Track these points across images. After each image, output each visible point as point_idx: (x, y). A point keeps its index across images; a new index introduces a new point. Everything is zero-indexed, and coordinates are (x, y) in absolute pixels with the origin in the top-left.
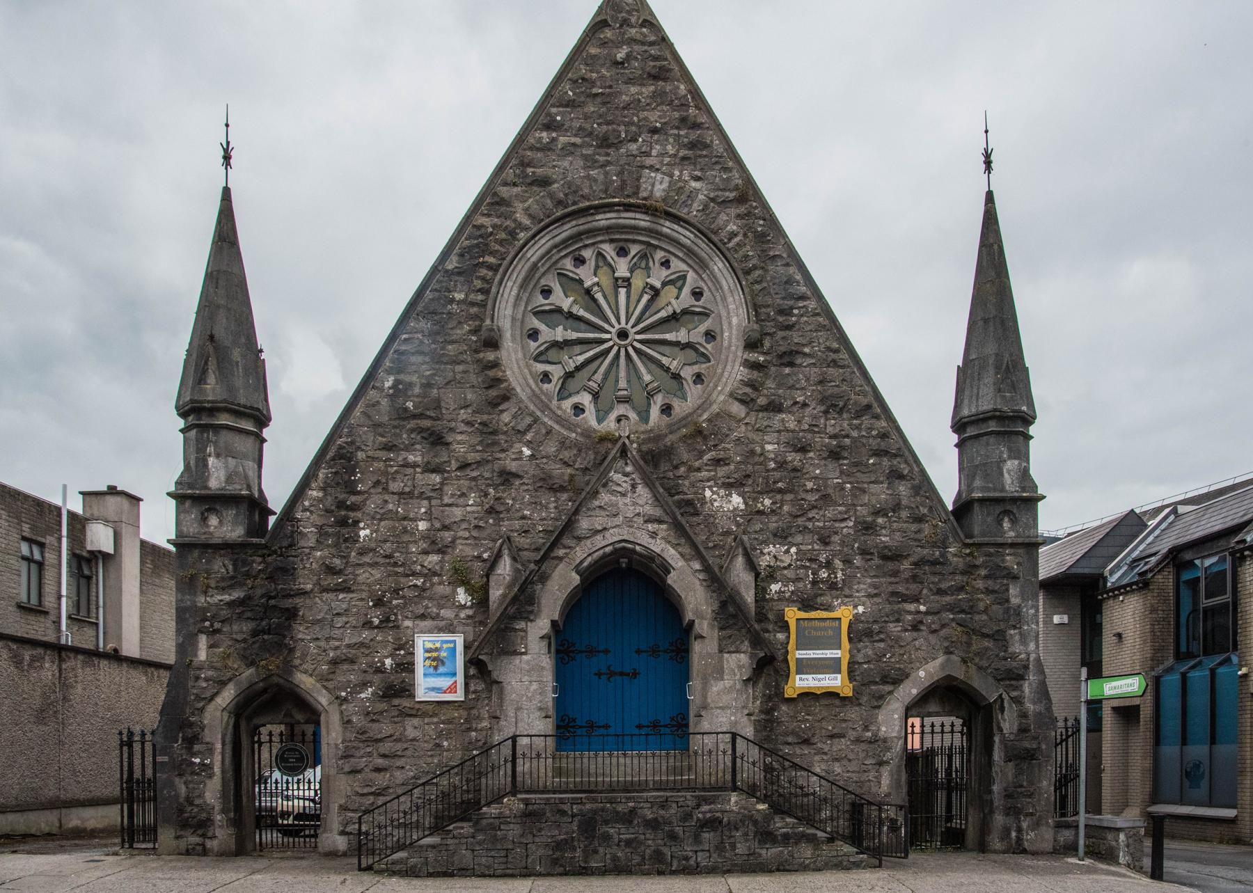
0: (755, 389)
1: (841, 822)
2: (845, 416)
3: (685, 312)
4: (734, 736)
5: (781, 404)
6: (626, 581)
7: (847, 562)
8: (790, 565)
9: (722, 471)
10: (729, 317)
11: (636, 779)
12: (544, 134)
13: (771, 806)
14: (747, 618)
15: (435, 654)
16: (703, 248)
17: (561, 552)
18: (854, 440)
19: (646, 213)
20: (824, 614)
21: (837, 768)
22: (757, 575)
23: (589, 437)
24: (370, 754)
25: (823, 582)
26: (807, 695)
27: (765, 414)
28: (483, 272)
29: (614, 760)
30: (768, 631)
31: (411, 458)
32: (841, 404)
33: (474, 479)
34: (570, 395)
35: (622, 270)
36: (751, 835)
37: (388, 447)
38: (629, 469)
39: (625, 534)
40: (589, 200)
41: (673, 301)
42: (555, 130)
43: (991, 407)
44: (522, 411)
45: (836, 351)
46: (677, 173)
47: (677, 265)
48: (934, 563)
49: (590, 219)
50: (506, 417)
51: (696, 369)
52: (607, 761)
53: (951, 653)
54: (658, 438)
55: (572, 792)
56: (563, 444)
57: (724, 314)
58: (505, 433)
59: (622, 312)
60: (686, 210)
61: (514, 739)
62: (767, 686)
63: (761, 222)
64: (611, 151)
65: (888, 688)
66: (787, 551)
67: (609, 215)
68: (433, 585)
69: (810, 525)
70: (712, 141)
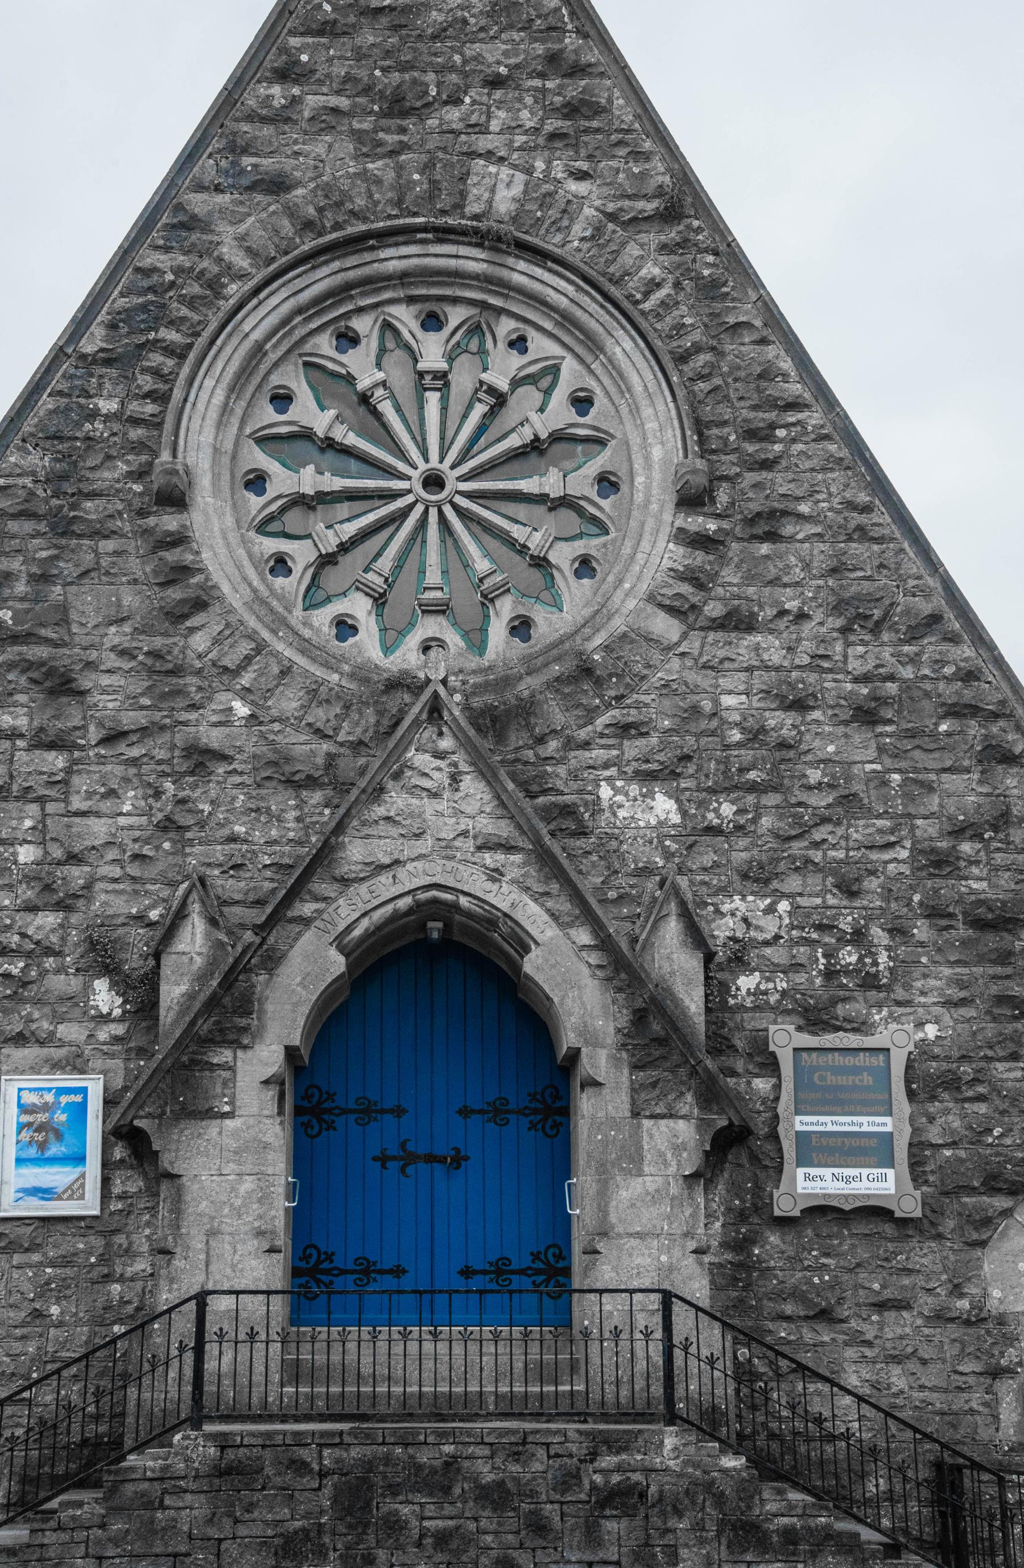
0: (699, 585)
1: (913, 1507)
2: (886, 637)
3: (558, 437)
4: (668, 1298)
5: (753, 615)
6: (440, 968)
7: (898, 931)
8: (777, 937)
9: (633, 748)
10: (645, 446)
11: (458, 1390)
12: (276, 90)
14: (687, 1044)
15: (41, 1118)
16: (592, 312)
17: (307, 909)
18: (907, 686)
19: (479, 245)
20: (852, 1040)
21: (897, 1378)
22: (709, 958)
23: (365, 681)
25: (847, 973)
26: (822, 1212)
27: (720, 635)
28: (156, 359)
29: (413, 1347)
30: (733, 1073)
32: (877, 613)
33: (134, 762)
34: (328, 600)
35: (432, 352)
36: (712, 1528)
38: (446, 743)
39: (437, 871)
40: (365, 220)
41: (534, 417)
42: (296, 82)
44: (232, 630)
45: (866, 509)
46: (540, 165)
47: (541, 346)
49: (367, 257)
50: (200, 642)
51: (580, 547)
52: (398, 1349)
54: (506, 682)
55: (322, 1418)
56: (314, 694)
57: (635, 440)
58: (199, 672)
59: (432, 438)
60: (558, 238)
61: (201, 1299)
62: (735, 1189)
63: (710, 259)
64: (409, 123)
65: (1001, 1202)
66: (770, 910)
67: (405, 250)
68: (43, 973)
69: (817, 856)
70: (610, 101)
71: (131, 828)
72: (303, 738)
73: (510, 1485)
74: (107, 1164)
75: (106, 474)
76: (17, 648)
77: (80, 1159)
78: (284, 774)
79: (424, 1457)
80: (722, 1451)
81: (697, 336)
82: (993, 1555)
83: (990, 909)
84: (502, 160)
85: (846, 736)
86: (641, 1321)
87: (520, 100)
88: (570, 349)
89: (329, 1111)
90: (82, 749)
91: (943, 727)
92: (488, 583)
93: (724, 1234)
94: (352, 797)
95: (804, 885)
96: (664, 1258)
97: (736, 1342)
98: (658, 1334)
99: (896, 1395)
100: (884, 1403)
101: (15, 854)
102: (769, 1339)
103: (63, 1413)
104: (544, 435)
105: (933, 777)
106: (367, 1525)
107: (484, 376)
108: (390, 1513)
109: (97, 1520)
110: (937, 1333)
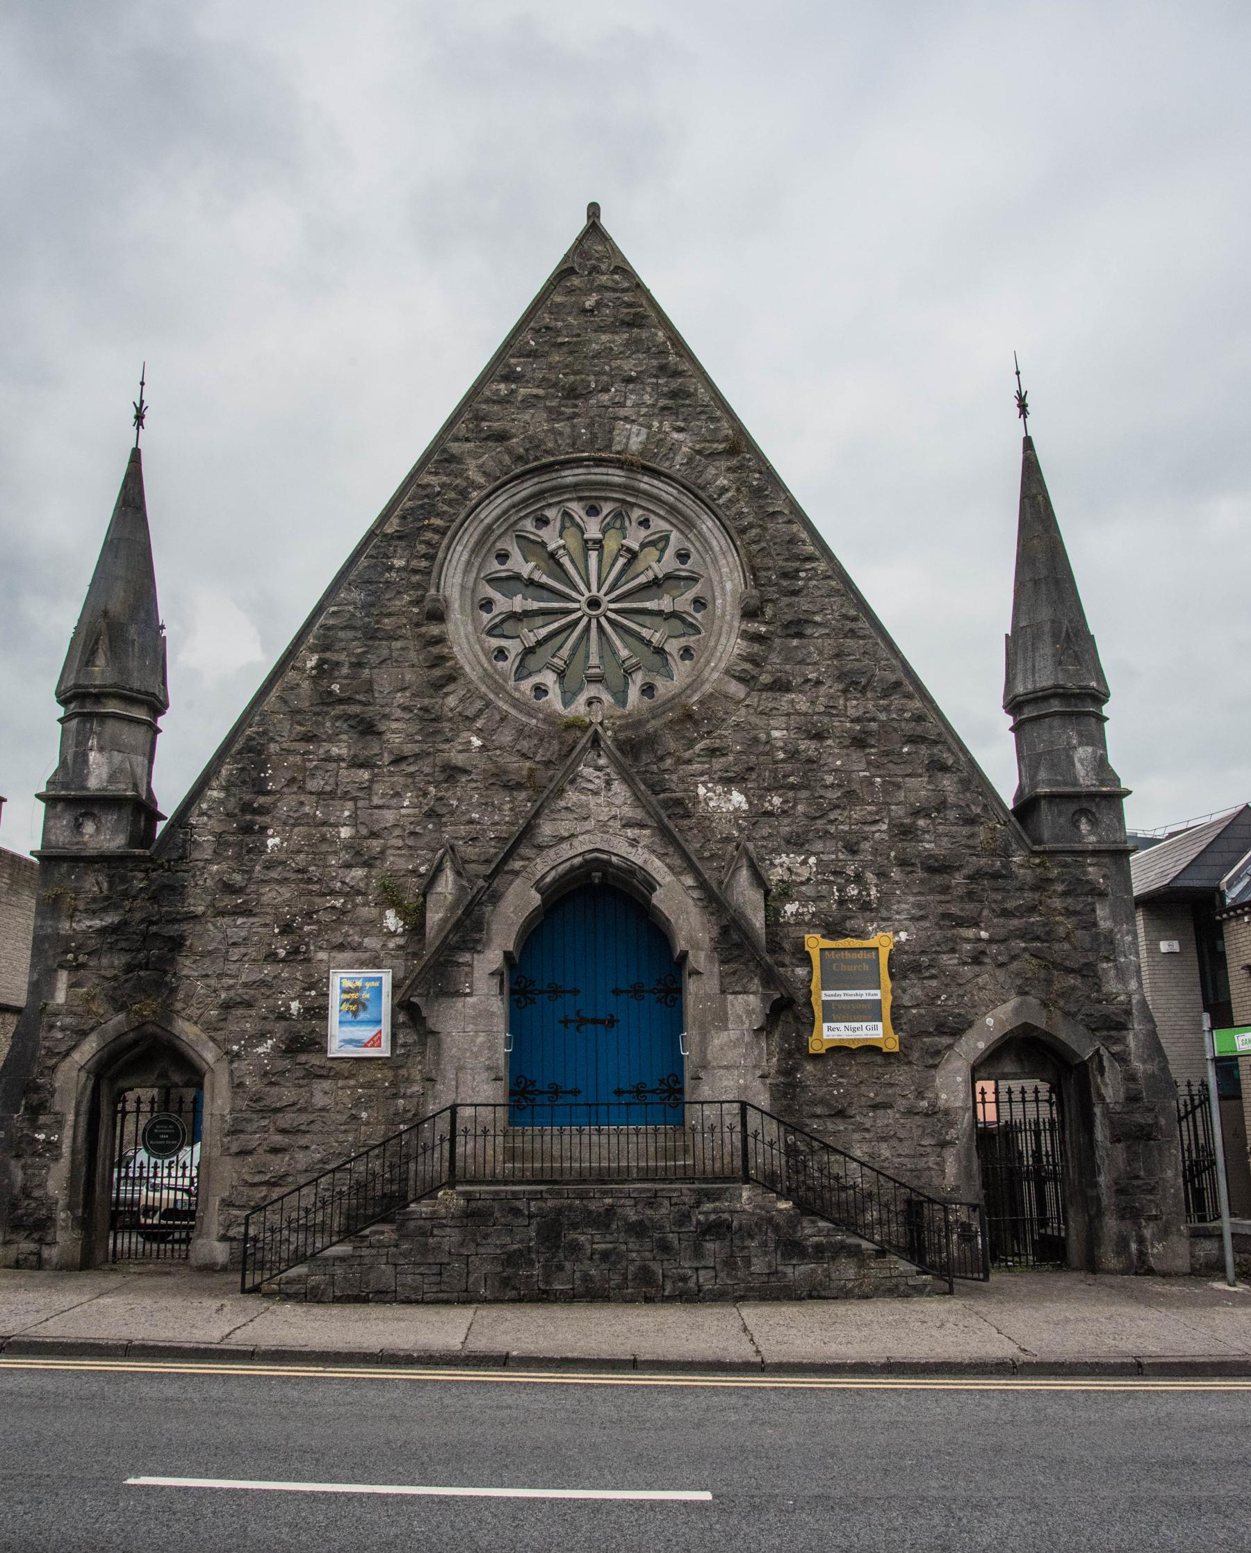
1: (894, 1227)
2: (869, 695)
3: (669, 577)
4: (744, 1106)
5: (789, 682)
6: (600, 900)
7: (882, 875)
8: (809, 879)
9: (718, 763)
11: (614, 1165)
12: (502, 386)
13: (797, 1205)
14: (754, 947)
15: (354, 996)
16: (688, 504)
17: (517, 865)
18: (883, 725)
19: (621, 468)
20: (856, 943)
22: (767, 893)
23: (552, 724)
24: (265, 1129)
25: (852, 901)
26: (839, 1051)
28: (428, 535)
29: (585, 1139)
30: (783, 965)
31: (335, 751)
32: (864, 681)
33: (411, 775)
34: (530, 675)
36: (772, 1245)
37: (308, 738)
39: (598, 841)
40: (553, 455)
41: (654, 565)
42: (514, 382)
43: (1050, 683)
44: (472, 694)
45: (855, 619)
46: (656, 424)
47: (658, 524)
48: (995, 876)
49: (554, 475)
50: (452, 701)
51: (683, 642)
52: (576, 1140)
53: (1026, 993)
54: (639, 723)
55: (529, 1183)
57: (715, 578)
58: (451, 719)
59: (593, 578)
61: (453, 1109)
62: (785, 1038)
63: (757, 475)
65: (946, 1040)
66: (804, 862)
68: (355, 906)
69: (832, 829)
70: (696, 390)
71: (409, 816)
72: (515, 759)
73: (646, 1222)
74: (394, 1025)
75: (397, 603)
76: (342, 707)
77: (379, 1022)
78: (504, 782)
79: (593, 1206)
80: (778, 1199)
81: (751, 519)
82: (940, 1252)
83: (936, 860)
84: (634, 421)
85: (848, 755)
86: (728, 1120)
87: (644, 389)
88: (675, 526)
89: (531, 992)
90: (379, 767)
91: (905, 750)
92: (627, 663)
93: (779, 1066)
94: (545, 795)
95: (825, 847)
96: (741, 1081)
97: (786, 1132)
98: (738, 1129)
99: (884, 1161)
100: (876, 1166)
101: (339, 833)
102: (807, 1130)
103: (370, 1178)
104: (660, 576)
105: (900, 779)
106: (559, 1247)
107: (624, 542)
108: (573, 1240)
109: (393, 1242)
110: (908, 1122)
